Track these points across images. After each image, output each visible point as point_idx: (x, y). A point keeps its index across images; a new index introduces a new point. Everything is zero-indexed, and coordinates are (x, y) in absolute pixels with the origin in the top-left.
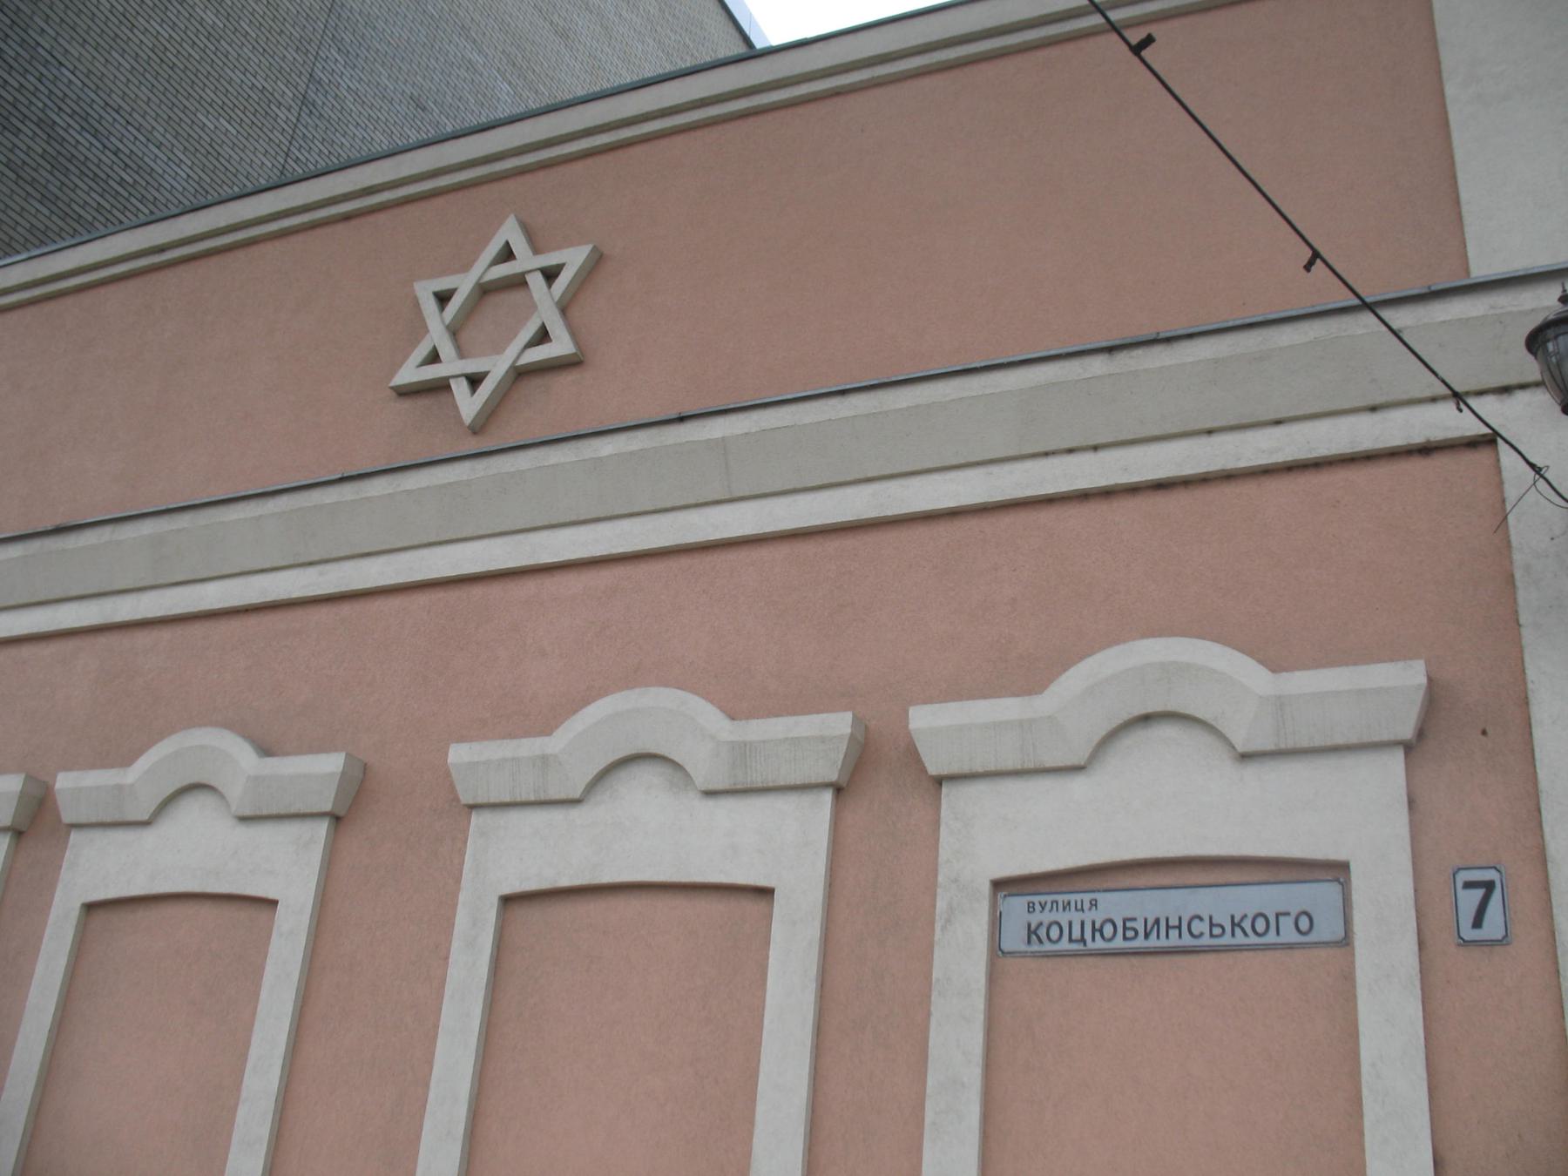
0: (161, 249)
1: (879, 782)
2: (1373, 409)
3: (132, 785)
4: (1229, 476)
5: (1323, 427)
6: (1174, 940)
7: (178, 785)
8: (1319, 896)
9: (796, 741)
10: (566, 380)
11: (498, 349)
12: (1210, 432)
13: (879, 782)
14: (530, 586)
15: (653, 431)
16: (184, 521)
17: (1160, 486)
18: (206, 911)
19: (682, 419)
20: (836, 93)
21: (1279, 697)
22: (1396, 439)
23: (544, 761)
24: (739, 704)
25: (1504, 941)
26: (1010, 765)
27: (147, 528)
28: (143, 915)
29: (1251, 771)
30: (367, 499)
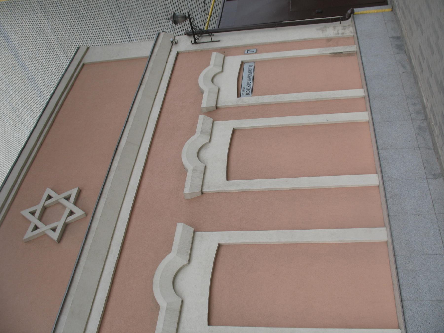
0: (63, 93)
1: (215, 112)
2: (167, 63)
3: (168, 303)
4: (170, 79)
5: (163, 83)
6: (252, 78)
7: (172, 281)
8: (246, 66)
9: (203, 124)
10: (83, 194)
11: (59, 220)
12: (161, 79)
13: (215, 112)
14: (142, 191)
15: (128, 123)
16: (70, 300)
17: (168, 86)
18: (218, 275)
19: (117, 150)
20: (41, 144)
21: (178, 252)
22: (173, 60)
23: (194, 170)
24: (192, 132)
25: (256, 50)
26: (216, 96)
27: (64, 318)
28: (215, 302)
29: (224, 70)
30: (97, 229)
